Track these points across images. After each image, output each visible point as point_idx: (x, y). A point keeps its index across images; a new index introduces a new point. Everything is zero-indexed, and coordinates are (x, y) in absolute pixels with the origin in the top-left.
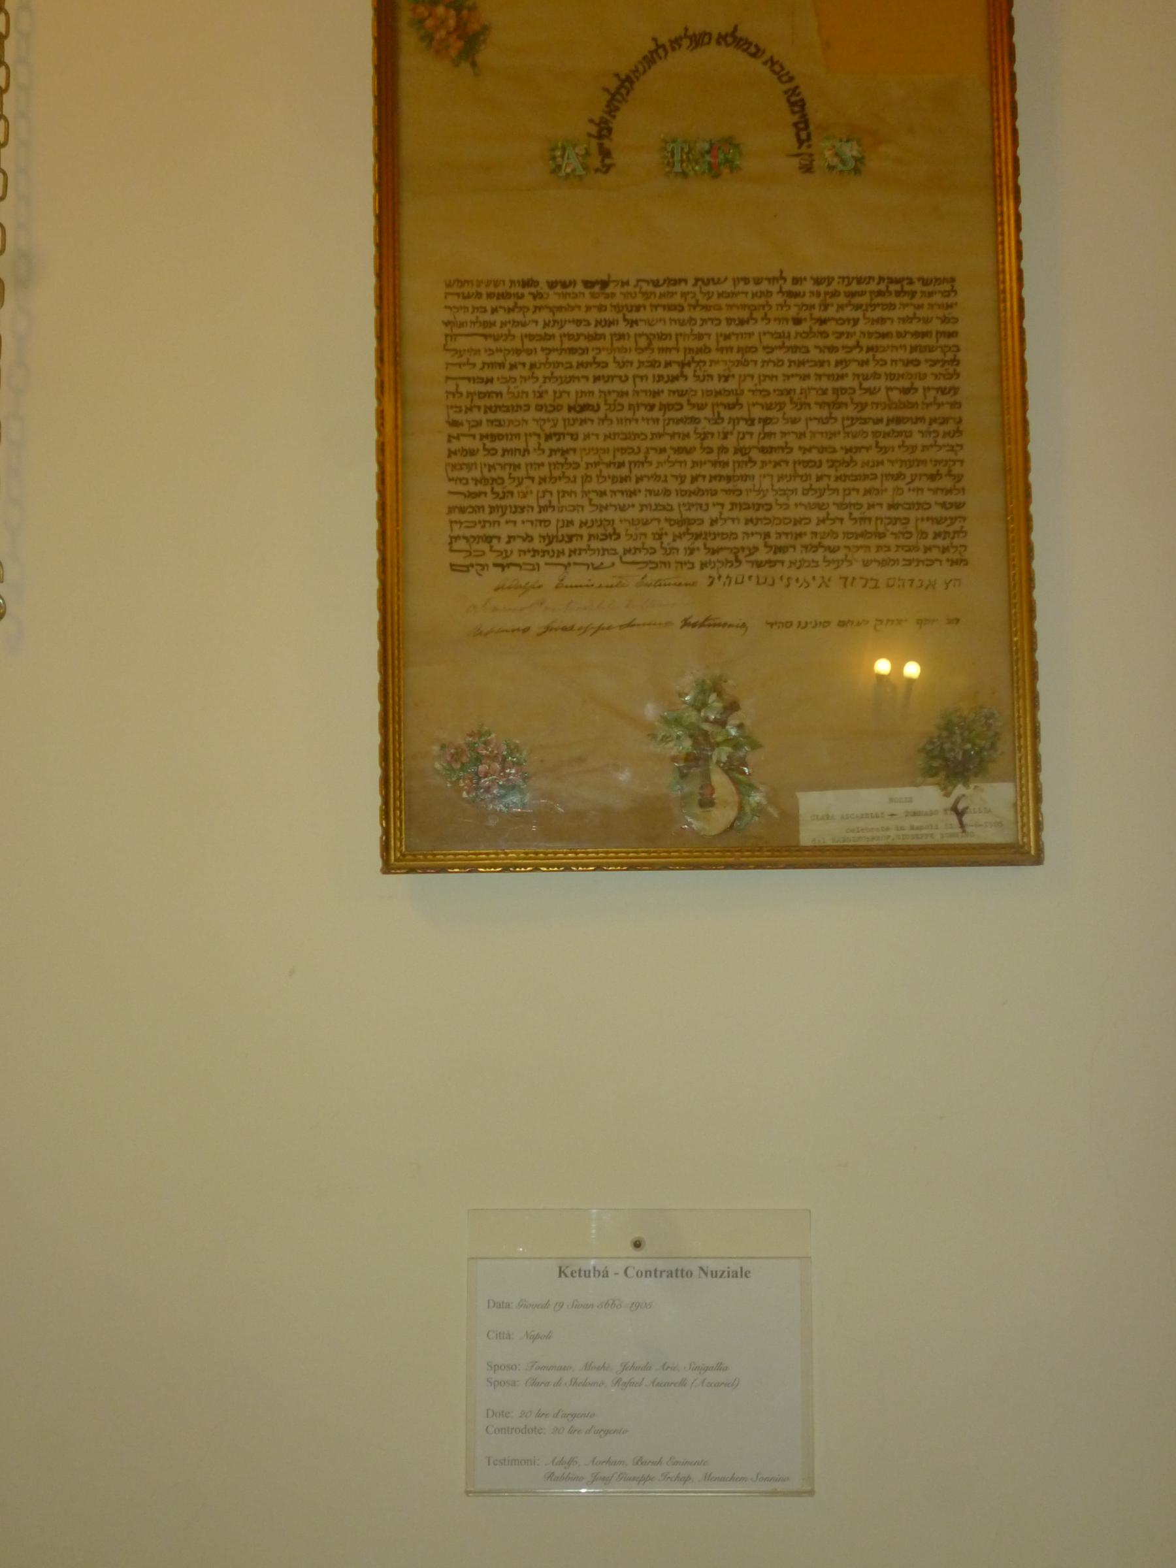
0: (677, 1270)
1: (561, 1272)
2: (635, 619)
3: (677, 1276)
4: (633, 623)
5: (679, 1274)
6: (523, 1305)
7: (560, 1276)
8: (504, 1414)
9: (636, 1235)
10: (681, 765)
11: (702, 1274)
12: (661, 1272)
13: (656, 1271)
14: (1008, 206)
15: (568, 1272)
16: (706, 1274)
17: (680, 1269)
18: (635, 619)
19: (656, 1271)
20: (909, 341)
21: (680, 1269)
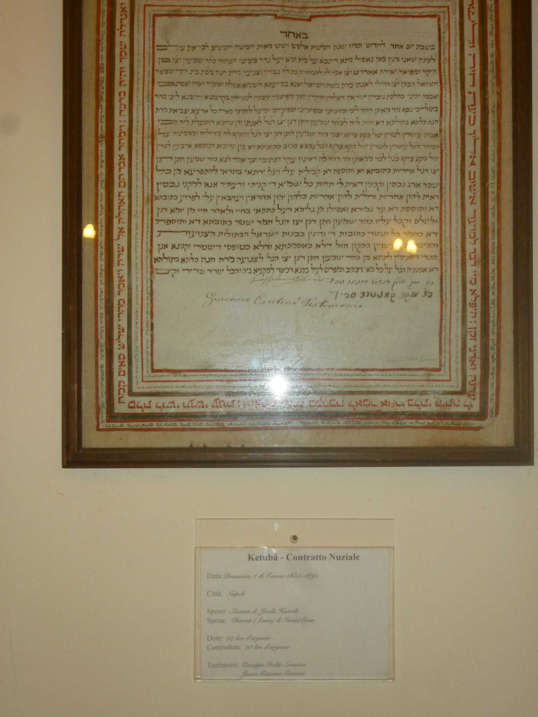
0: (317, 556)
6: (228, 576)
7: (249, 560)
8: (218, 639)
13: (305, 556)
15: (254, 557)
16: (334, 558)
17: (319, 555)
21: (319, 555)
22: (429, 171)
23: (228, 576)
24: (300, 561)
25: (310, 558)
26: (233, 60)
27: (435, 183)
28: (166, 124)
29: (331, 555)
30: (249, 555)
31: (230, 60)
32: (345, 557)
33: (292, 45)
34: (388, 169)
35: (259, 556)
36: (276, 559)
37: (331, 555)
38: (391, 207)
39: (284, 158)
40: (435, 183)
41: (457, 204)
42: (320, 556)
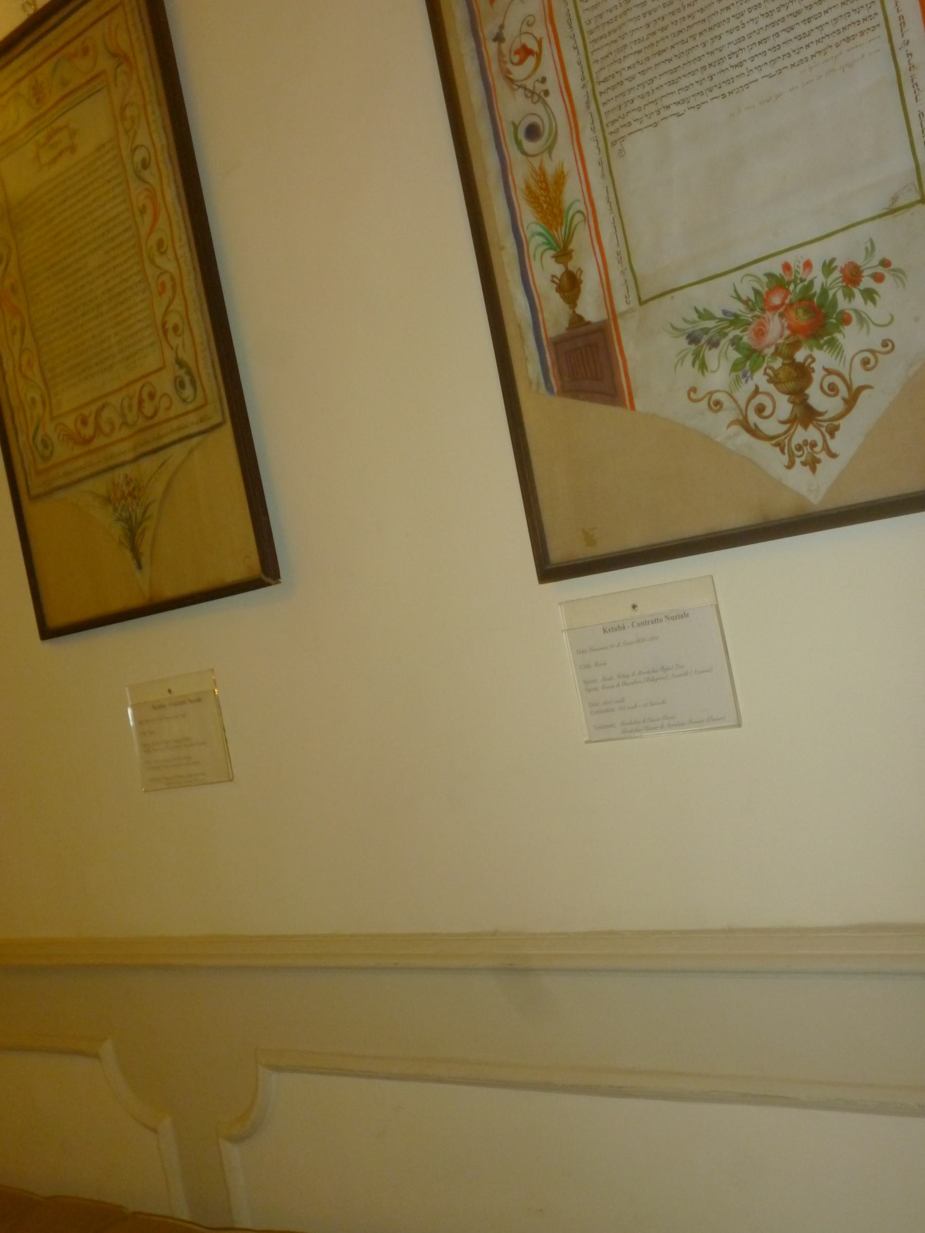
0: (655, 620)
1: (604, 631)
2: (731, 296)
3: (656, 623)
4: (736, 296)
5: (656, 621)
6: (592, 650)
7: (604, 633)
8: (596, 704)
9: (631, 604)
10: (815, 300)
11: (667, 620)
12: (648, 622)
13: (646, 622)
14: (548, 108)
15: (607, 630)
16: (669, 619)
17: (656, 618)
18: (731, 296)
19: (646, 622)
20: (770, 56)
21: (656, 618)
22: (700, 45)
23: (592, 650)
24: (643, 626)
25: (650, 623)
26: (696, 71)
27: (910, 48)
28: (579, 173)
29: (666, 616)
30: (603, 629)
31: (693, 72)
32: (678, 617)
33: (620, 37)
34: (788, 54)
35: (611, 628)
36: (624, 628)
37: (666, 616)
38: (730, 91)
39: (755, 68)
40: (910, 48)
41: (901, 18)
42: (657, 619)
